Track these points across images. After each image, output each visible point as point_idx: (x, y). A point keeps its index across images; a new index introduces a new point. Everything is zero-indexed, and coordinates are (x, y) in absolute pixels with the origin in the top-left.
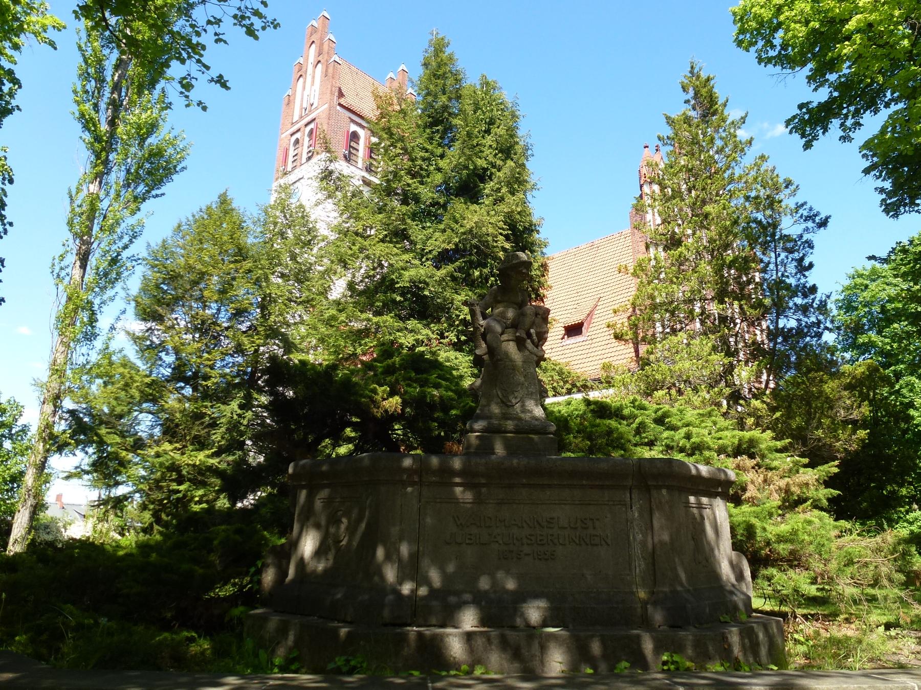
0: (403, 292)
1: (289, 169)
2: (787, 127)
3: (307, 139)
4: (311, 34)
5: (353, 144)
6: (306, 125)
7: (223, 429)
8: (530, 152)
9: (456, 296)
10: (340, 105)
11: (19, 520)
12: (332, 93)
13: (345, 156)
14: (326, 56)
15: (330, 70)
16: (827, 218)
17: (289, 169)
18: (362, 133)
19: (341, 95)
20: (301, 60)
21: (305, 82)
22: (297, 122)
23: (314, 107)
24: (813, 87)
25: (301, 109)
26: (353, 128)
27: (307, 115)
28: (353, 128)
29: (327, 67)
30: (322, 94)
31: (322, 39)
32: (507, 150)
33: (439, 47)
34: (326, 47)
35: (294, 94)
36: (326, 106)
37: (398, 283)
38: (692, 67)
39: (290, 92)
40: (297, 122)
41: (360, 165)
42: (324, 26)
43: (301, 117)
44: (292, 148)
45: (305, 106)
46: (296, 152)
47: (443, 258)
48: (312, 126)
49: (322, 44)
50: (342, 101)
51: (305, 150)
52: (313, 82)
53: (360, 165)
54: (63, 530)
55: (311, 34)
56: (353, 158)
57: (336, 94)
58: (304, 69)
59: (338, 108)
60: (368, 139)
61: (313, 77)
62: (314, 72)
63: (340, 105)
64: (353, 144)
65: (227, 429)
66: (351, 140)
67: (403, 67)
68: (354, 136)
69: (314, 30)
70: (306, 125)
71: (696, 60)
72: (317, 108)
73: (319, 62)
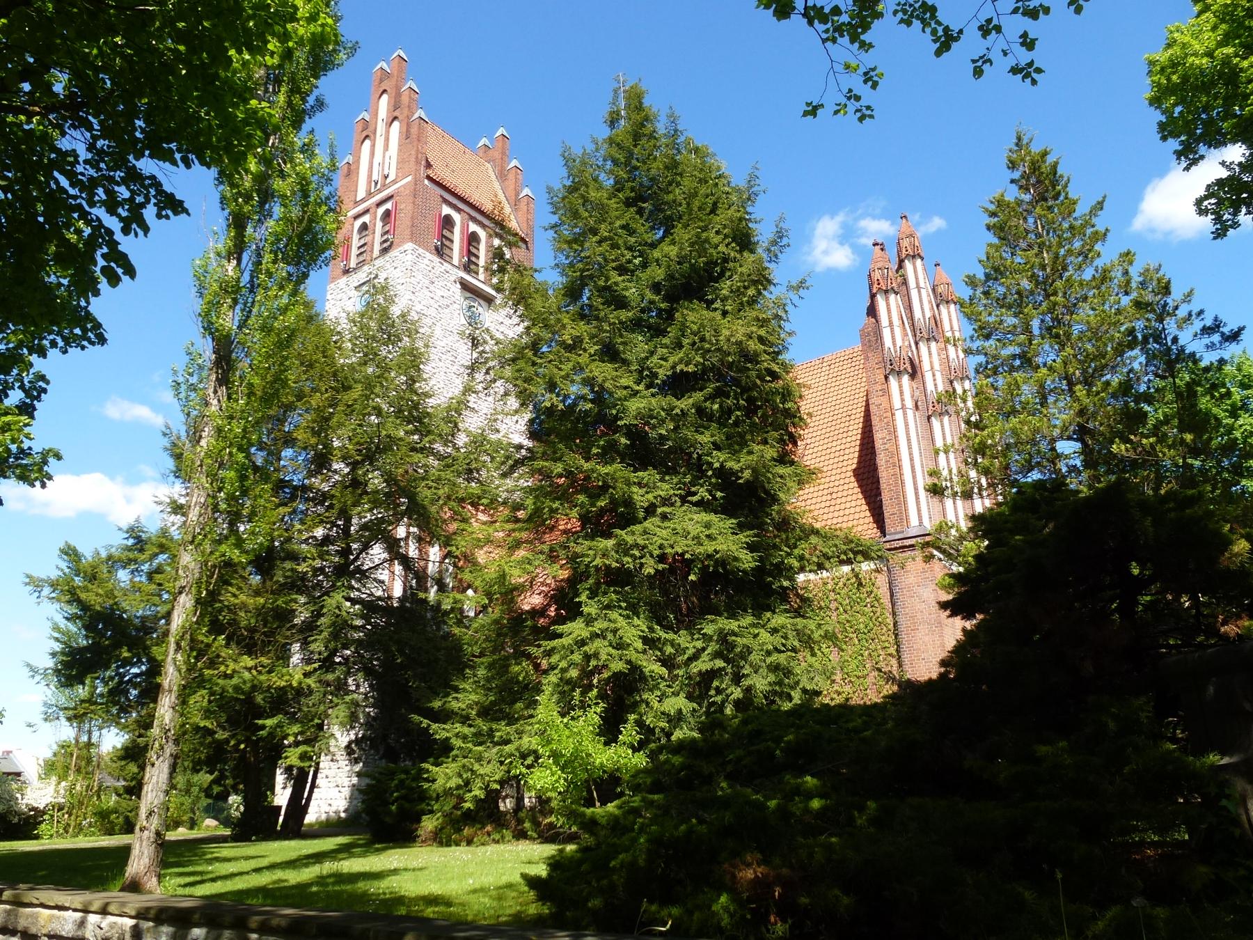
0: (631, 432)
1: (353, 265)
2: (441, 252)
3: (379, 224)
4: (381, 81)
5: (445, 232)
6: (379, 204)
7: (325, 634)
8: (785, 241)
9: (700, 438)
10: (428, 178)
11: (154, 779)
12: (418, 162)
13: (437, 249)
14: (406, 112)
15: (414, 130)
16: (1241, 329)
17: (353, 265)
18: (456, 217)
19: (429, 165)
20: (367, 116)
21: (373, 146)
22: (363, 200)
23: (388, 180)
24: (1184, 165)
25: (369, 182)
26: (446, 210)
27: (380, 191)
28: (446, 210)
29: (409, 126)
30: (401, 162)
31: (398, 88)
32: (744, 241)
33: (636, 101)
34: (405, 99)
35: (357, 161)
36: (409, 178)
37: (621, 419)
38: (1019, 139)
39: (350, 158)
40: (363, 200)
41: (456, 261)
42: (400, 70)
43: (370, 194)
44: (356, 236)
45: (375, 177)
46: (362, 242)
47: (678, 384)
48: (389, 205)
49: (398, 95)
50: (429, 172)
51: (378, 239)
52: (386, 147)
53: (456, 261)
54: (18, 796)
55: (381, 81)
56: (447, 251)
57: (423, 163)
58: (371, 128)
59: (426, 182)
60: (465, 227)
61: (387, 140)
62: (388, 132)
63: (428, 178)
64: (445, 232)
65: (331, 634)
66: (444, 227)
67: (501, 131)
68: (447, 222)
69: (385, 75)
70: (379, 204)
71: (1024, 128)
72: (394, 182)
73: (395, 118)
